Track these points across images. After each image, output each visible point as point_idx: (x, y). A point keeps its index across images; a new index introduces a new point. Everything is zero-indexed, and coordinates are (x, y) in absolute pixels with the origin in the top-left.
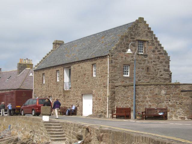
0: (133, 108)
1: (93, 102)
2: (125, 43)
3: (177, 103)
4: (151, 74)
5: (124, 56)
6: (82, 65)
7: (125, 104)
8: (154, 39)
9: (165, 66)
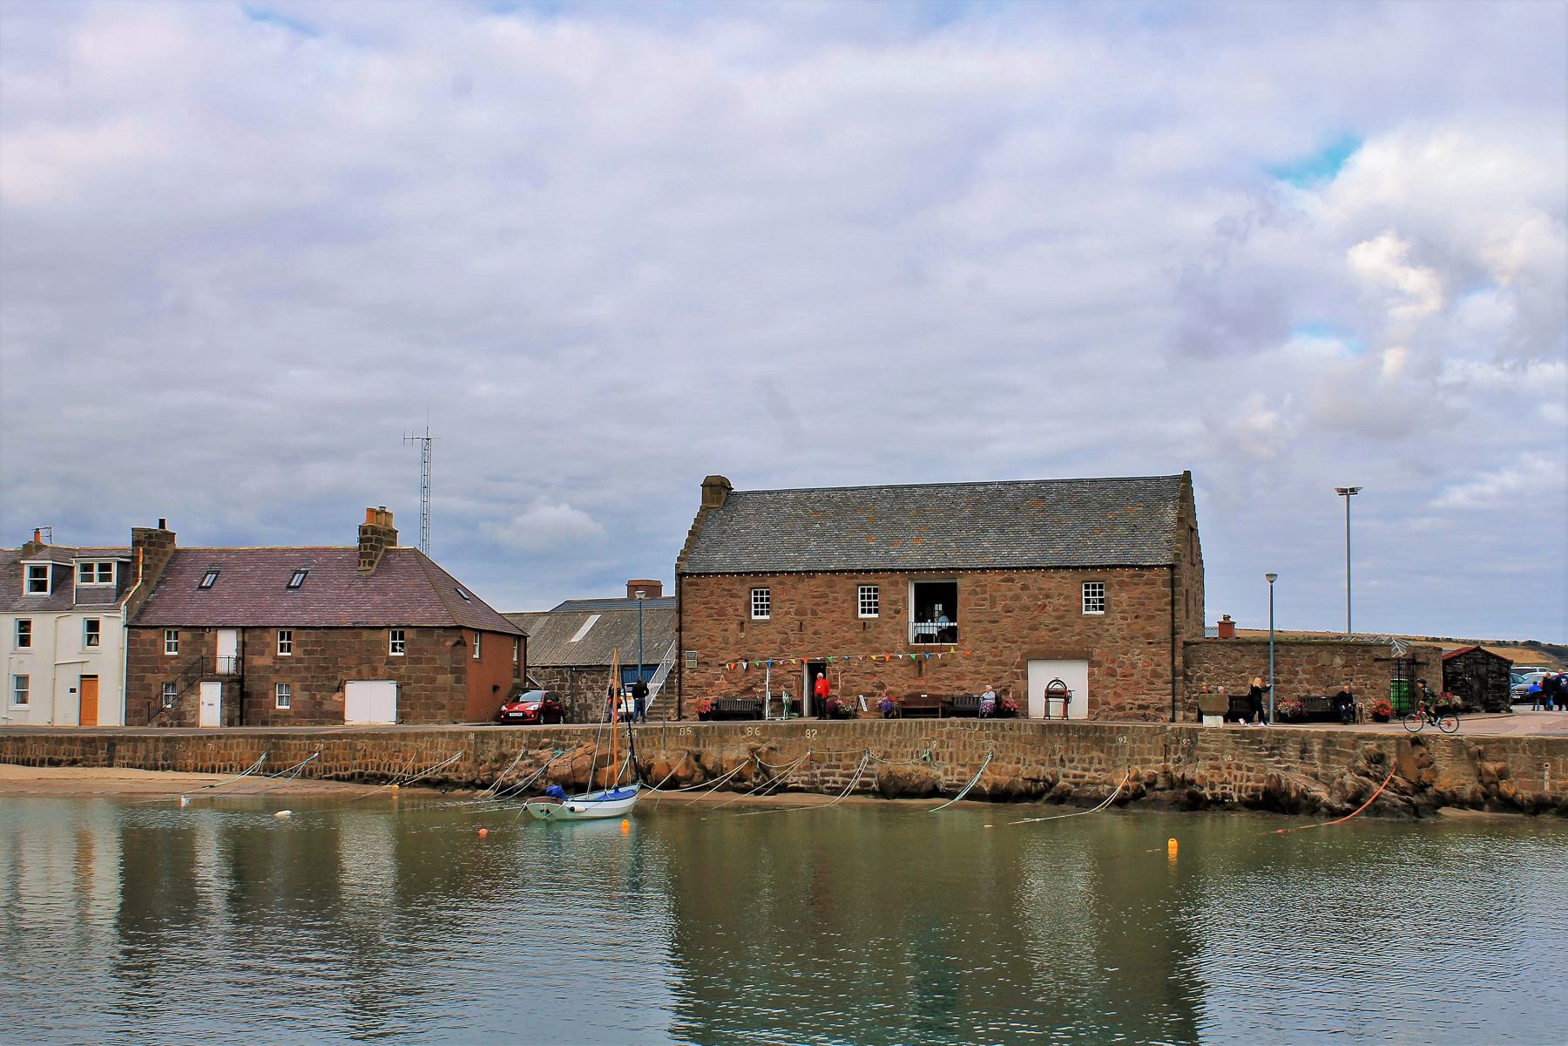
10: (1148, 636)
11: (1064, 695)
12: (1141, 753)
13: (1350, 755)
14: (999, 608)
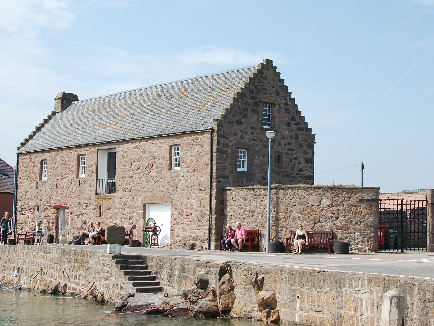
0: (265, 232)
1: (173, 220)
2: (242, 107)
3: (351, 221)
4: (283, 167)
5: (239, 132)
6: (143, 144)
7: (247, 224)
8: (289, 101)
9: (307, 153)
14: (133, 167)
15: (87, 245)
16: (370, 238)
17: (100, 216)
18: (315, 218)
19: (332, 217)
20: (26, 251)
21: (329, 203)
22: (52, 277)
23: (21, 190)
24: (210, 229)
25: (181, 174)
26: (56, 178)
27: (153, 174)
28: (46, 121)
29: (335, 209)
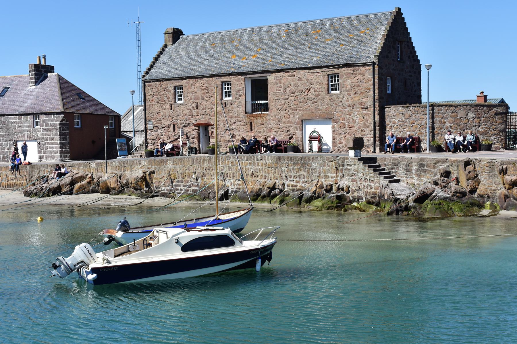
1: (333, 132)
3: (489, 129)
10: (361, 104)
11: (319, 139)
12: (324, 172)
13: (432, 173)
14: (288, 91)
15: (332, 152)
16: (502, 139)
17: (251, 130)
18: (464, 127)
19: (476, 125)
20: (232, 159)
21: (474, 116)
22: (265, 178)
23: (151, 111)
24: (375, 137)
25: (341, 96)
26: (196, 101)
27: (311, 96)
28: (161, 53)
29: (478, 120)
